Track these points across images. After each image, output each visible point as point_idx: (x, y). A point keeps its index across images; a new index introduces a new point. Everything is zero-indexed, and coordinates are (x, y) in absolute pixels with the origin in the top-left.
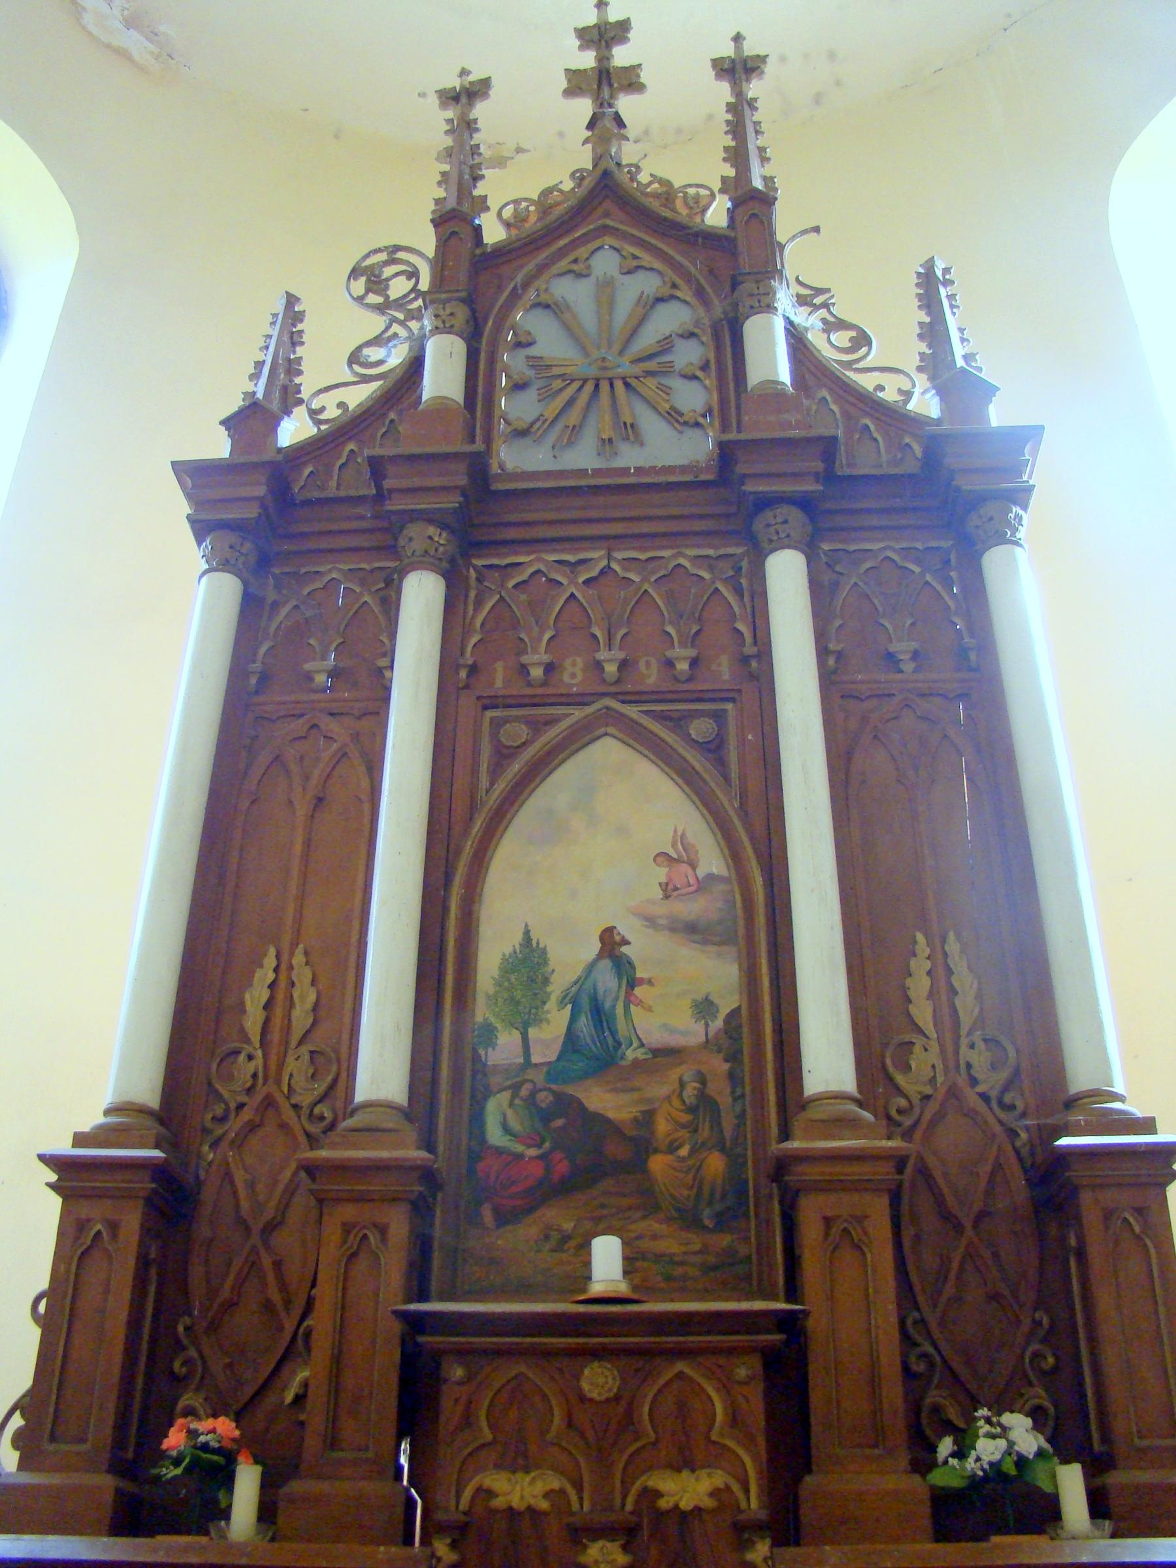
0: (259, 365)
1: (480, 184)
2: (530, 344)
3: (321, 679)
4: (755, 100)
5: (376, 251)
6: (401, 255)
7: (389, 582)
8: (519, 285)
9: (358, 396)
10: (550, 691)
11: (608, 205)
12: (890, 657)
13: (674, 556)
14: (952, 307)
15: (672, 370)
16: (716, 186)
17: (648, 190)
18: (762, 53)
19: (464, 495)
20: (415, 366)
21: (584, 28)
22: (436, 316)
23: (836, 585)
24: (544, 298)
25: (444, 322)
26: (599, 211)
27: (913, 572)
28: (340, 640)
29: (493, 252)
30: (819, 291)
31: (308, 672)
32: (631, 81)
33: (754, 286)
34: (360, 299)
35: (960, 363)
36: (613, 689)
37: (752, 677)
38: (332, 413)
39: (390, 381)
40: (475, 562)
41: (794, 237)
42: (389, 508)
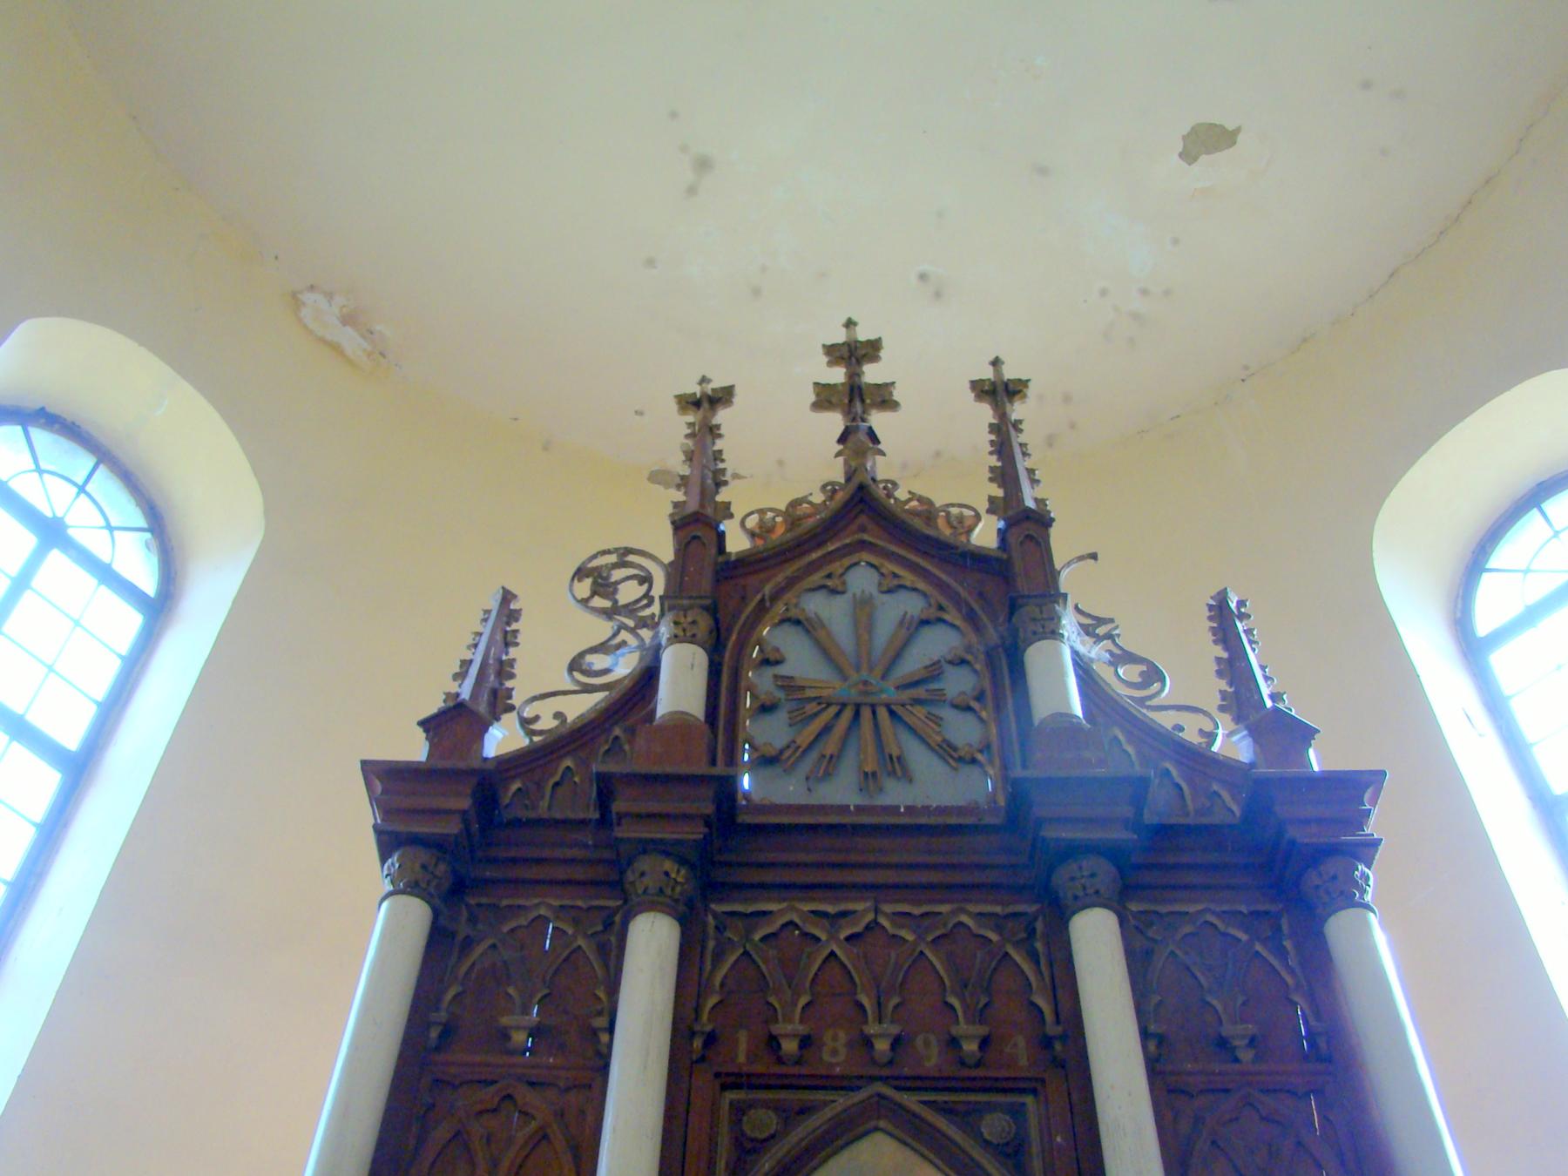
0: (466, 664)
1: (723, 490)
2: (778, 662)
3: (519, 1038)
4: (1020, 422)
5: (604, 553)
6: (631, 558)
7: (608, 925)
8: (767, 597)
9: (578, 707)
10: (804, 1070)
11: (863, 519)
12: (1223, 1043)
13: (954, 913)
14: (1251, 642)
15: (943, 698)
16: (982, 506)
17: (907, 507)
18: (1024, 378)
19: (708, 824)
20: (648, 678)
21: (833, 345)
22: (676, 623)
23: (1149, 953)
24: (793, 613)
25: (684, 630)
26: (854, 527)
27: (1239, 940)
28: (546, 991)
29: (737, 561)
30: (1100, 621)
31: (506, 1028)
32: (884, 398)
33: (1037, 610)
34: (584, 602)
35: (1269, 704)
36: (886, 1072)
37: (1061, 1065)
38: (547, 723)
39: (616, 694)
40: (713, 906)
41: (1069, 564)
42: (619, 835)
